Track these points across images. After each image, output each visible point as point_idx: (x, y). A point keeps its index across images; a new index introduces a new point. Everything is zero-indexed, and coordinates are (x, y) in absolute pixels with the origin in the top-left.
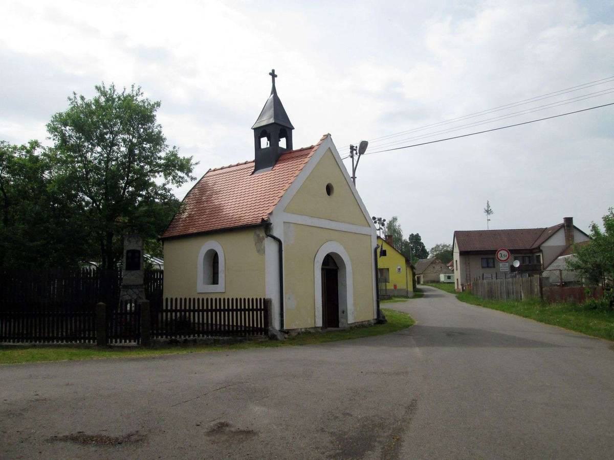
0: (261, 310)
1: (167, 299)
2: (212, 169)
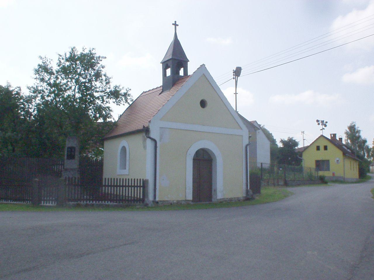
1: (105, 179)
2: (145, 91)
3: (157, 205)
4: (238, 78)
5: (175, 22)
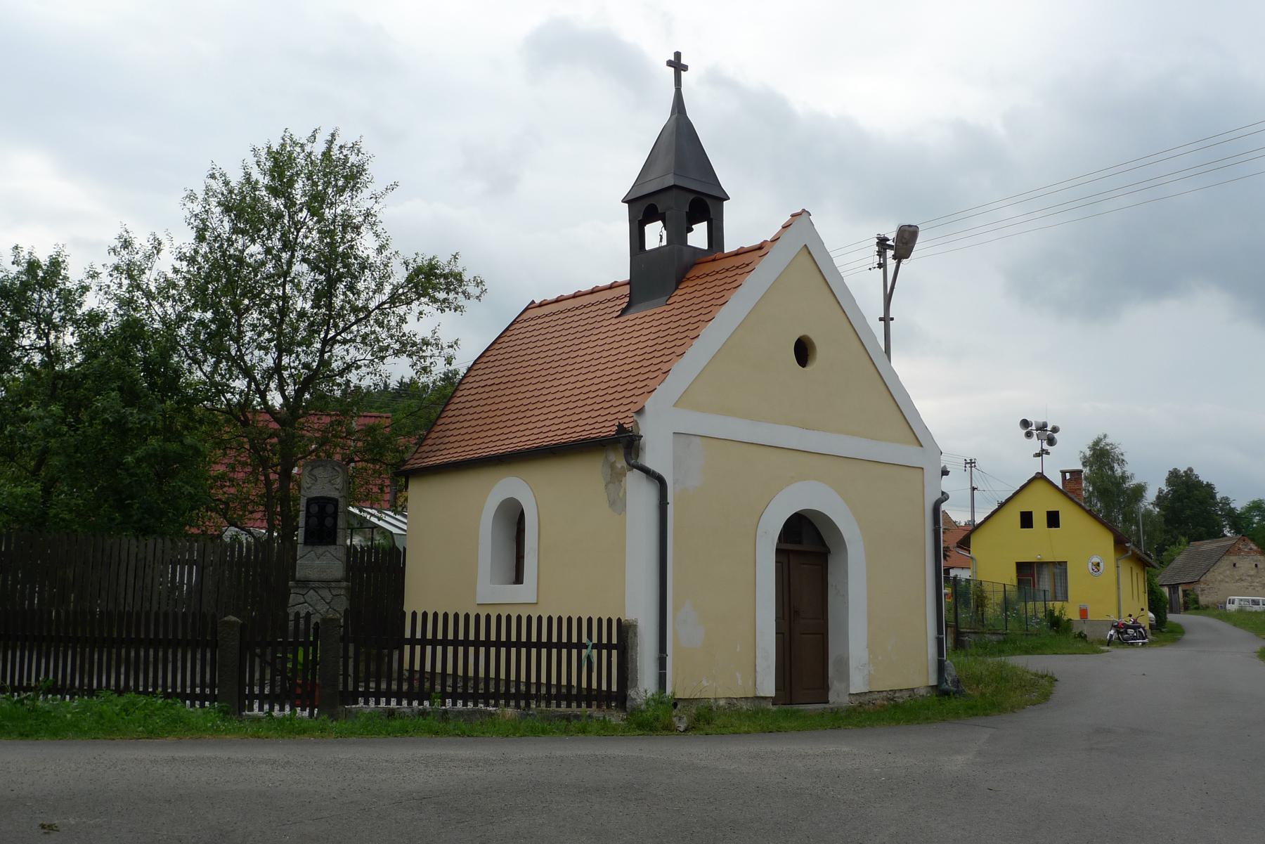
1: (414, 614)
2: (537, 302)
3: (662, 718)
5: (678, 55)
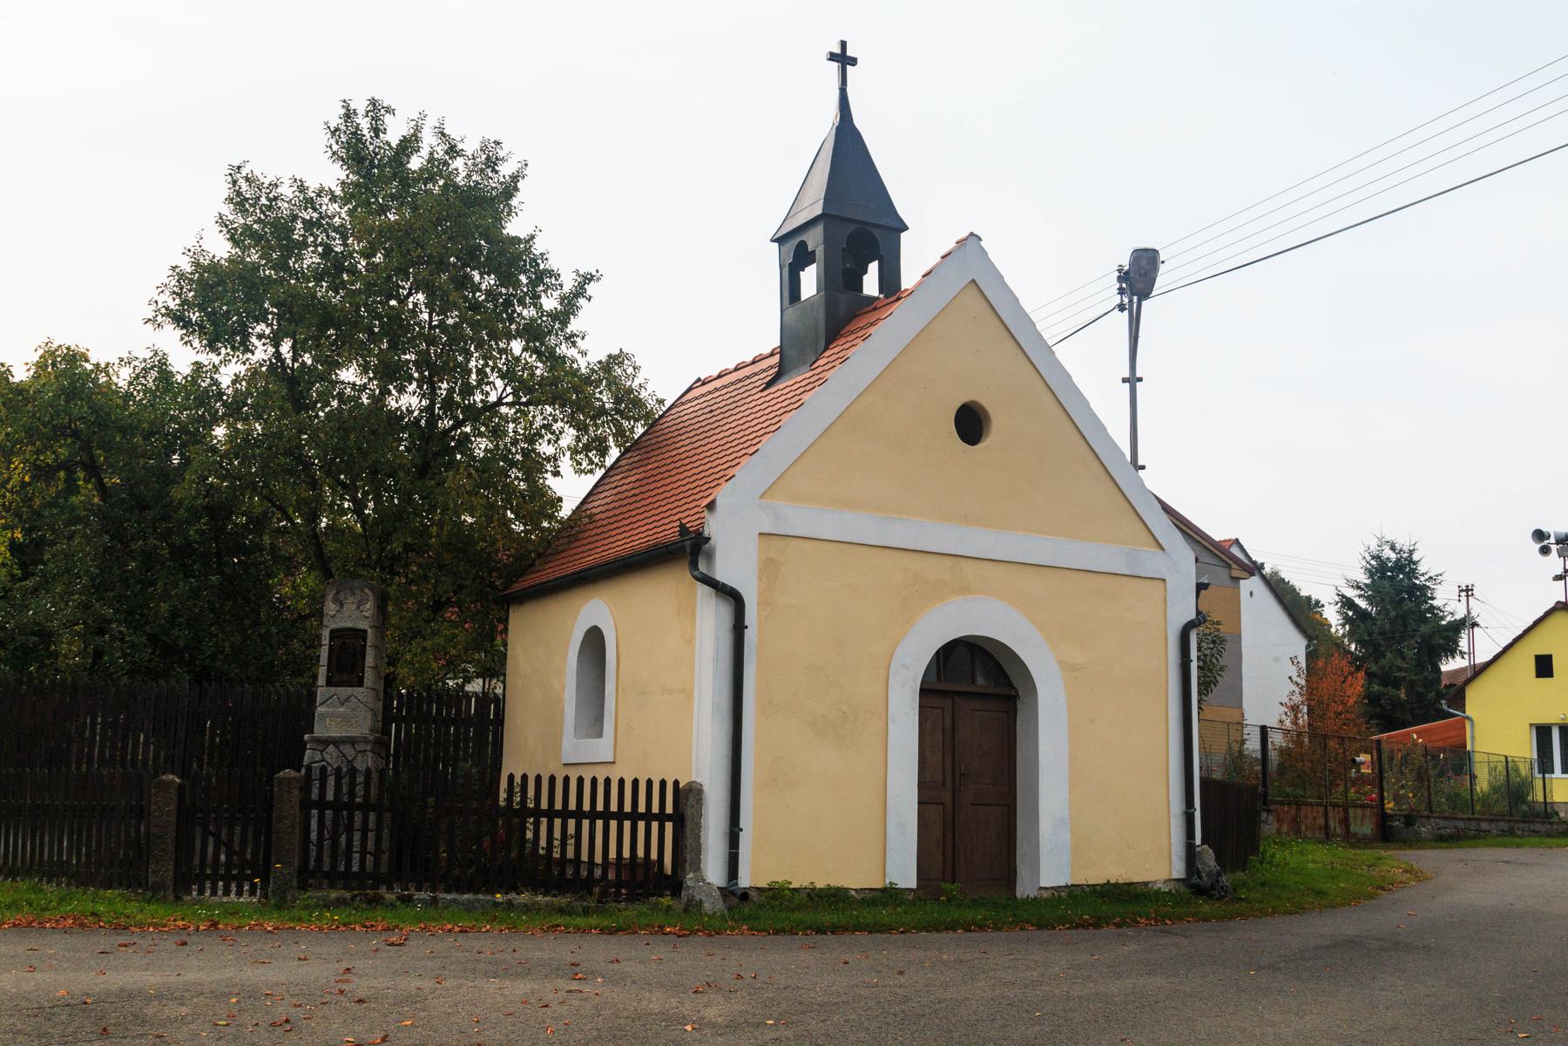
0: (662, 818)
1: (511, 777)
4: (1144, 303)
5: (843, 44)
